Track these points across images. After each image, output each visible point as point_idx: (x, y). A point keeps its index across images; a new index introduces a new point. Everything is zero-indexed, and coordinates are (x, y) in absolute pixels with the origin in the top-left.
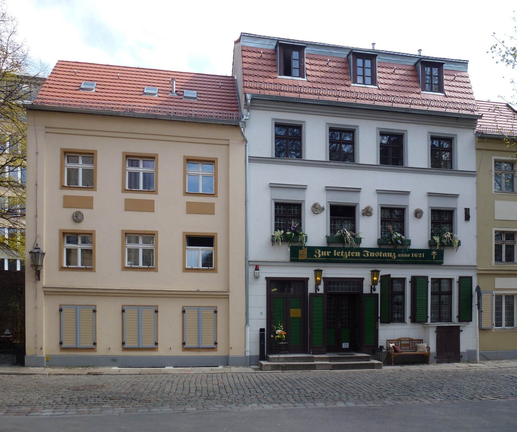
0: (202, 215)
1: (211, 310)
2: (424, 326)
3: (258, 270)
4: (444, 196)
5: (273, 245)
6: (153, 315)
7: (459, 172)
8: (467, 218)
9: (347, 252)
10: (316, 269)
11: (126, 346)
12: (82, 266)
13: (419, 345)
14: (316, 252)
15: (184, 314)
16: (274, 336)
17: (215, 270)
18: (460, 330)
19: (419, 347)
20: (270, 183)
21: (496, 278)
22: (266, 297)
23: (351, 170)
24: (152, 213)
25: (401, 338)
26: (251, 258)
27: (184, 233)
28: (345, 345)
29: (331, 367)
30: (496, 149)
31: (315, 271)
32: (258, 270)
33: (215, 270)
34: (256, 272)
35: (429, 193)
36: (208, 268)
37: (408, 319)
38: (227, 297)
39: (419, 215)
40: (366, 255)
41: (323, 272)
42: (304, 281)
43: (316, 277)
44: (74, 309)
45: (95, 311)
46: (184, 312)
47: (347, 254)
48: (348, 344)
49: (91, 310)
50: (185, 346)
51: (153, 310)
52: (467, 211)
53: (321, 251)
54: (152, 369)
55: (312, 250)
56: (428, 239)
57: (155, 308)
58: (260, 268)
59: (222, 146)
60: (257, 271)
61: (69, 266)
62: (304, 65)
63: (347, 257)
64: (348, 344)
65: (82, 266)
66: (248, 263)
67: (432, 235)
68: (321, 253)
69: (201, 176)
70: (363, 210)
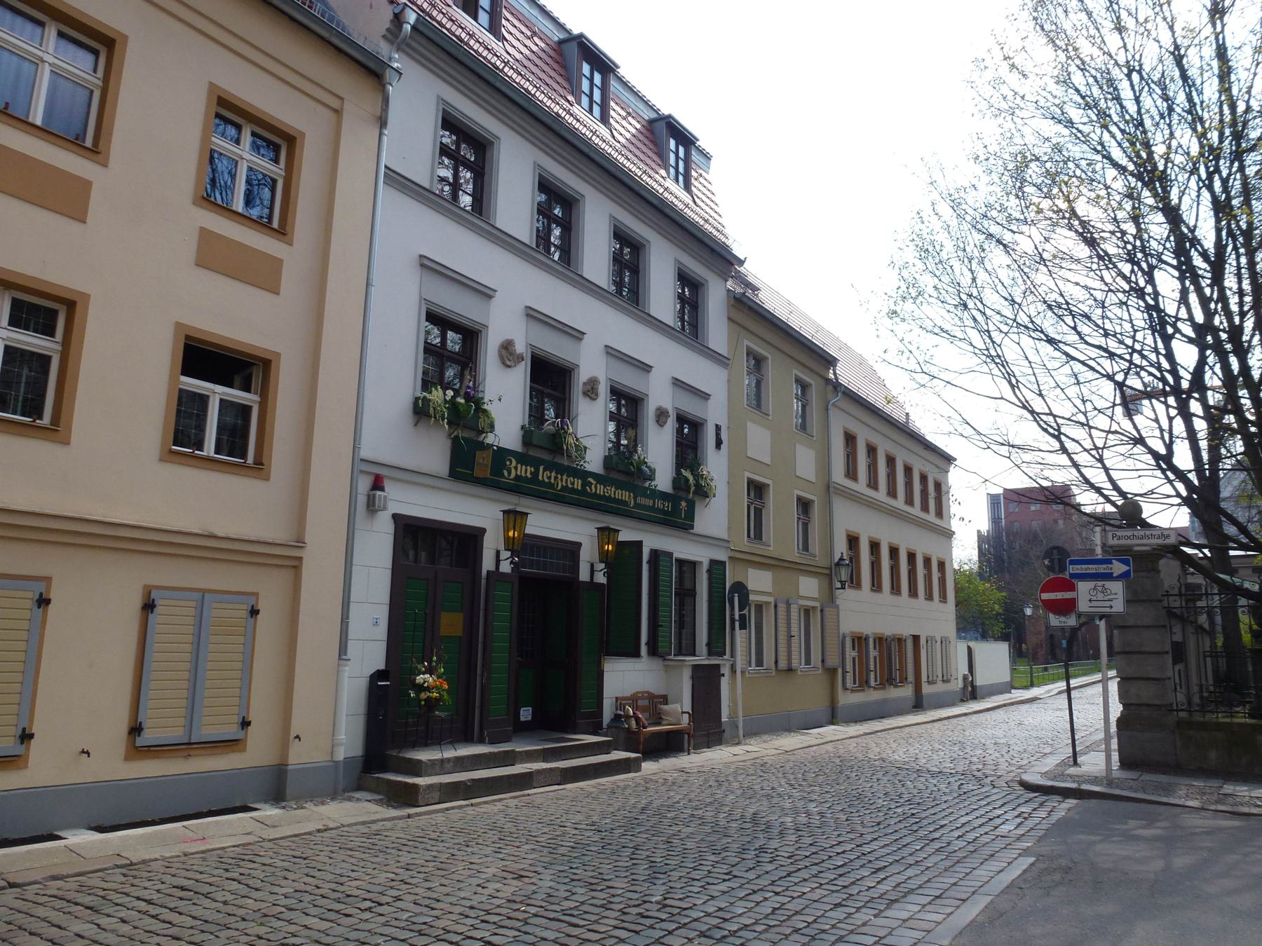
0: (71, 221)
1: (238, 606)
2: (666, 663)
3: (382, 489)
4: (681, 387)
5: (416, 425)
6: (27, 614)
7: (709, 352)
8: (719, 444)
9: (562, 475)
10: (506, 508)
11: (148, 737)
12: (216, 453)
13: (665, 707)
14: (508, 463)
15: (151, 616)
16: (418, 695)
17: (260, 468)
18: (722, 672)
19: (667, 713)
20: (421, 253)
21: (749, 569)
22: (389, 573)
23: (602, 303)
24: (74, 226)
25: (637, 692)
26: (365, 453)
27: (278, 355)
28: (526, 714)
29: (559, 778)
30: (234, 30)
31: (504, 512)
32: (382, 489)
33: (260, 468)
34: (380, 495)
35: (676, 379)
36: (193, 452)
37: (644, 650)
38: (295, 566)
39: (663, 419)
40: (591, 490)
41: (530, 519)
42: (469, 539)
43: (506, 530)
44: (193, 604)
45: (43, 602)
46: (149, 607)
47: (562, 480)
48: (530, 708)
49: (245, 607)
50: (140, 742)
51: (30, 595)
52: (718, 428)
53: (517, 463)
54: (28, 852)
55: (501, 455)
56: (605, 452)
57: (40, 587)
58: (387, 485)
59: (320, 108)
60: (378, 493)
61: (196, 452)
62: (501, 11)
63: (559, 487)
64: (530, 708)
65: (216, 453)
66: (360, 464)
67: (426, 385)
68: (516, 468)
69: (47, 69)
70: (585, 384)
